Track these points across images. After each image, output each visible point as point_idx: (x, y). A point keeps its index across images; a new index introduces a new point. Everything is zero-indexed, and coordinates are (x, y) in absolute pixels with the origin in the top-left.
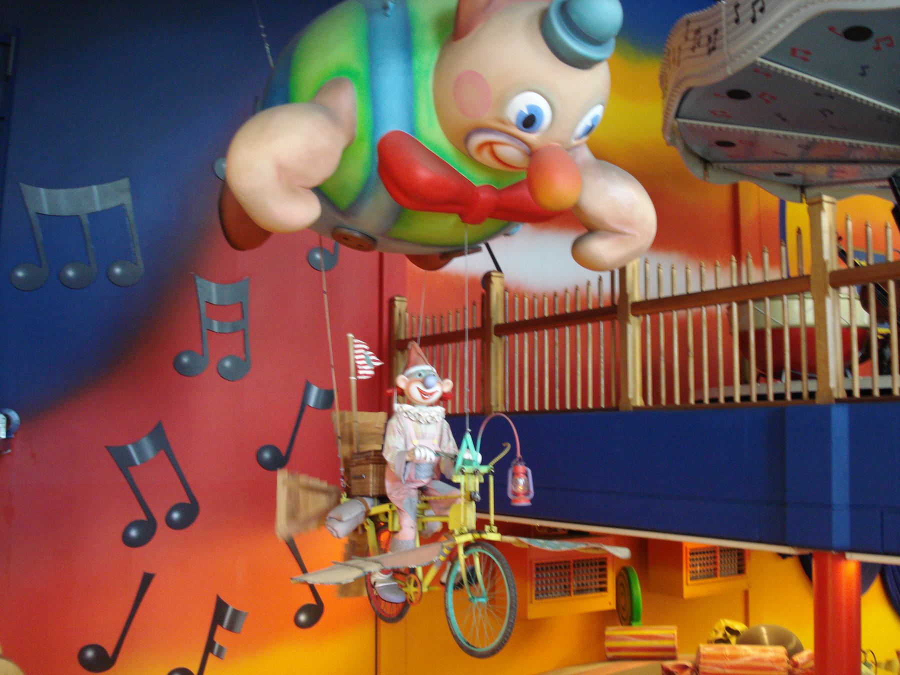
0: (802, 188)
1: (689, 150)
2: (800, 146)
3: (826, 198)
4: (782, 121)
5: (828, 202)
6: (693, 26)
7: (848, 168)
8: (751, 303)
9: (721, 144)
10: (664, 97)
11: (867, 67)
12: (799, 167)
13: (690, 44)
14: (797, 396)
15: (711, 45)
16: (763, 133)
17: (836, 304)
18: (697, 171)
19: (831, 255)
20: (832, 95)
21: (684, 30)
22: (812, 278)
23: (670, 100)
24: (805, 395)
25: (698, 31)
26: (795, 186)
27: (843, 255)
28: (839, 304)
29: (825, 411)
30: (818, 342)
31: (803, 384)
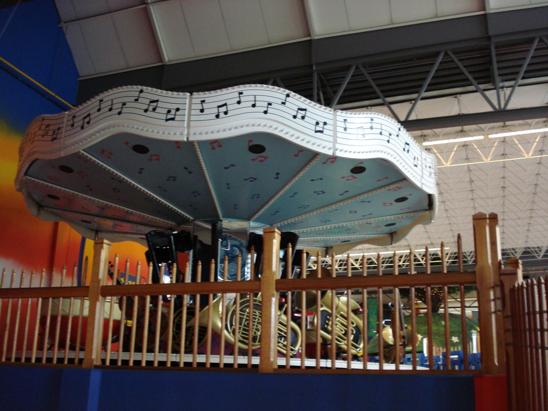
0: (97, 232)
1: (30, 196)
2: (98, 207)
3: (105, 241)
4: (89, 190)
5: (106, 244)
6: (46, 122)
7: (124, 224)
8: (51, 300)
9: (51, 196)
10: (20, 161)
11: (143, 169)
12: (97, 219)
13: (41, 132)
14: (71, 361)
15: (55, 136)
16: (189, 227)
17: (103, 305)
18: (34, 211)
19: (104, 276)
20: (121, 181)
21: (40, 123)
22: (90, 289)
23: (23, 163)
24: (76, 361)
25: (48, 126)
26: (92, 230)
27: (111, 275)
28: (104, 305)
29: (87, 372)
30: (89, 328)
31: (76, 353)
